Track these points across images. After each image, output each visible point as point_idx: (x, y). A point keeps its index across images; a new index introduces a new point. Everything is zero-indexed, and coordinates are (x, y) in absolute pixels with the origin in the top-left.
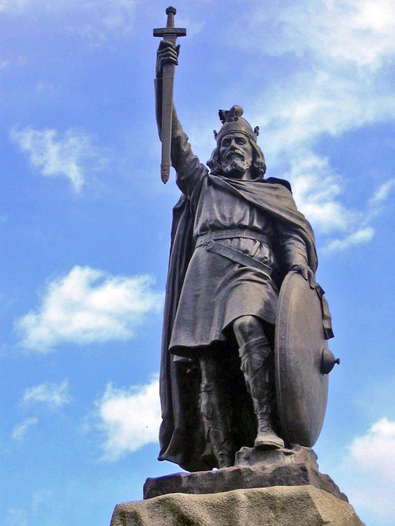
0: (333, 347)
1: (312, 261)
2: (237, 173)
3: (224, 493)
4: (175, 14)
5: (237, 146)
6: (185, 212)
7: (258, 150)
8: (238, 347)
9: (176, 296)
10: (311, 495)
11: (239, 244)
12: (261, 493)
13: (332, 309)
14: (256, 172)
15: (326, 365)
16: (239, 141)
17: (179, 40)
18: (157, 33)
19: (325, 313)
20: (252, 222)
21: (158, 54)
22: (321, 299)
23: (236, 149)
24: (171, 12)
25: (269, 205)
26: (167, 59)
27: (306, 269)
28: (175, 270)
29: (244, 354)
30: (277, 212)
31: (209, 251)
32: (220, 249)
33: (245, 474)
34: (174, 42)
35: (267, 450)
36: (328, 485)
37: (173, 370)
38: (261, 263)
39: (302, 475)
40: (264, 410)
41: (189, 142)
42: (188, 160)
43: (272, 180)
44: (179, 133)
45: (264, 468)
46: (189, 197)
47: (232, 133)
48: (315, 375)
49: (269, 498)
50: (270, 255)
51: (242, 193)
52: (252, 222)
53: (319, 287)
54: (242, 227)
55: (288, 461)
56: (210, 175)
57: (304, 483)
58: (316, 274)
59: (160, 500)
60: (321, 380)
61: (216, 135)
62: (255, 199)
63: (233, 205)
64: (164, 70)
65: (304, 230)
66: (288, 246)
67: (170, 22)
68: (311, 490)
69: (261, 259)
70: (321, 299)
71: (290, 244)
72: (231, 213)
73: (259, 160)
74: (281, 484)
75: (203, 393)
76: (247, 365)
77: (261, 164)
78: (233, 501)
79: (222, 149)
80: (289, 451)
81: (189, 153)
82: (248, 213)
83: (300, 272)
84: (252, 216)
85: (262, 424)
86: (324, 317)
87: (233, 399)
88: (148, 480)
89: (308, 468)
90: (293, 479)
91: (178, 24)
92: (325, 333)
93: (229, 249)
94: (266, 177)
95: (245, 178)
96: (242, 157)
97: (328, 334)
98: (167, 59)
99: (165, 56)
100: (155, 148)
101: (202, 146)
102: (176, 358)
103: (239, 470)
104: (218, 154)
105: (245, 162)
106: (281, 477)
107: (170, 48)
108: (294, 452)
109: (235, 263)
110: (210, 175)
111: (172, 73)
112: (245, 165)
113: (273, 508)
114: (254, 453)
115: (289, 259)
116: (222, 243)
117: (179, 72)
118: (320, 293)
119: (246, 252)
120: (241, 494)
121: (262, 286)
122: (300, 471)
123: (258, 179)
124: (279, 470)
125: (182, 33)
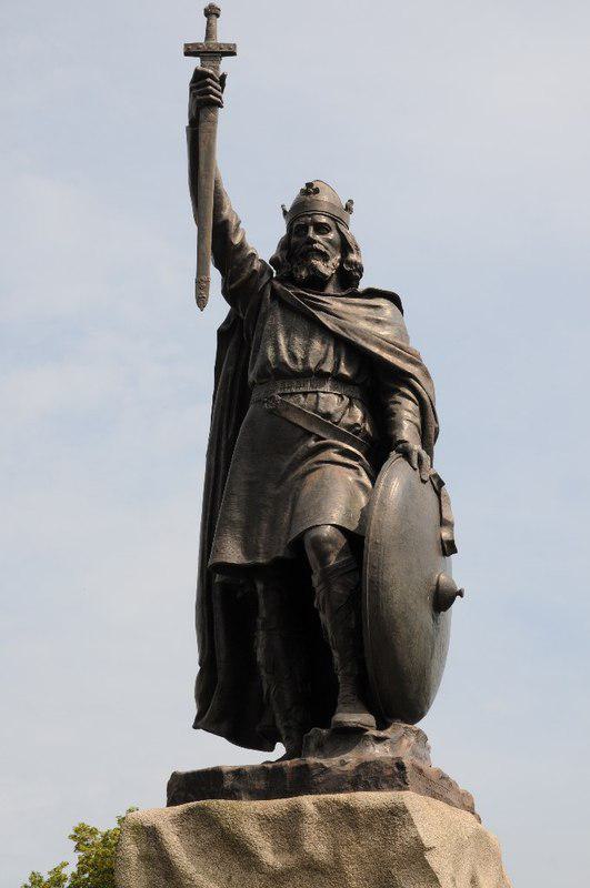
0: (457, 571)
1: (428, 434)
2: (318, 283)
3: (284, 800)
4: (218, 16)
5: (318, 237)
6: (236, 342)
7: (349, 239)
8: (311, 572)
9: (222, 472)
10: (409, 807)
11: (317, 403)
12: (337, 803)
13: (454, 511)
14: (348, 278)
15: (443, 599)
16: (322, 229)
17: (226, 65)
18: (190, 51)
19: (444, 516)
20: (337, 365)
21: (191, 89)
22: (438, 494)
23: (315, 242)
24: (211, 13)
25: (364, 339)
26: (205, 96)
27: (416, 446)
28: (220, 429)
29: (319, 584)
30: (376, 350)
31: (271, 412)
32: (287, 409)
33: (315, 772)
34: (216, 68)
35: (354, 735)
36: (439, 788)
37: (217, 592)
38: (351, 434)
39: (395, 775)
40: (348, 670)
41: (241, 226)
42: (238, 257)
43: (372, 293)
44: (226, 213)
45: (343, 763)
46: (241, 315)
47: (309, 216)
48: (425, 613)
49: (348, 811)
50: (364, 420)
51: (321, 316)
52: (337, 365)
53: (436, 476)
54: (321, 376)
55: (377, 752)
56: (278, 285)
57: (401, 788)
58: (436, 448)
59: (190, 809)
60: (435, 619)
61: (285, 213)
62: (343, 329)
63: (309, 337)
64: (202, 116)
65: (418, 381)
66: (392, 406)
67: (209, 34)
68: (411, 799)
69: (350, 427)
70: (438, 494)
71: (396, 402)
72: (306, 353)
73: (353, 257)
74: (367, 788)
75: (261, 633)
76: (323, 600)
77: (355, 264)
78: (297, 814)
79: (294, 239)
80: (382, 734)
81: (242, 246)
82: (331, 349)
83: (406, 454)
84: (337, 355)
85: (345, 691)
86: (443, 523)
87: (307, 642)
88: (174, 775)
89: (406, 762)
90: (387, 782)
91: (223, 37)
92: (443, 548)
93: (300, 411)
94: (363, 286)
95: (330, 289)
96: (325, 257)
97: (449, 548)
98: (205, 96)
99: (200, 94)
100: (223, 117)
101: (263, 237)
102: (218, 578)
103: (306, 766)
104: (285, 245)
105: (330, 264)
106: (369, 777)
107: (209, 80)
108: (389, 736)
109: (309, 434)
110: (275, 283)
111: (214, 122)
112: (327, 268)
113: (354, 825)
114: (330, 738)
115: (395, 428)
116: (291, 401)
117: (227, 124)
118: (438, 485)
119: (328, 415)
120: (308, 802)
121: (351, 471)
122: (396, 770)
123: (350, 290)
124: (364, 765)
125: (230, 52)
